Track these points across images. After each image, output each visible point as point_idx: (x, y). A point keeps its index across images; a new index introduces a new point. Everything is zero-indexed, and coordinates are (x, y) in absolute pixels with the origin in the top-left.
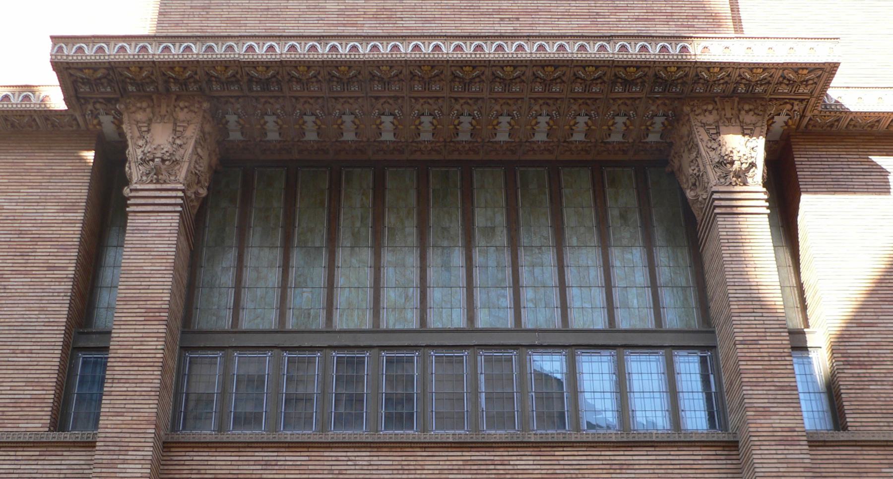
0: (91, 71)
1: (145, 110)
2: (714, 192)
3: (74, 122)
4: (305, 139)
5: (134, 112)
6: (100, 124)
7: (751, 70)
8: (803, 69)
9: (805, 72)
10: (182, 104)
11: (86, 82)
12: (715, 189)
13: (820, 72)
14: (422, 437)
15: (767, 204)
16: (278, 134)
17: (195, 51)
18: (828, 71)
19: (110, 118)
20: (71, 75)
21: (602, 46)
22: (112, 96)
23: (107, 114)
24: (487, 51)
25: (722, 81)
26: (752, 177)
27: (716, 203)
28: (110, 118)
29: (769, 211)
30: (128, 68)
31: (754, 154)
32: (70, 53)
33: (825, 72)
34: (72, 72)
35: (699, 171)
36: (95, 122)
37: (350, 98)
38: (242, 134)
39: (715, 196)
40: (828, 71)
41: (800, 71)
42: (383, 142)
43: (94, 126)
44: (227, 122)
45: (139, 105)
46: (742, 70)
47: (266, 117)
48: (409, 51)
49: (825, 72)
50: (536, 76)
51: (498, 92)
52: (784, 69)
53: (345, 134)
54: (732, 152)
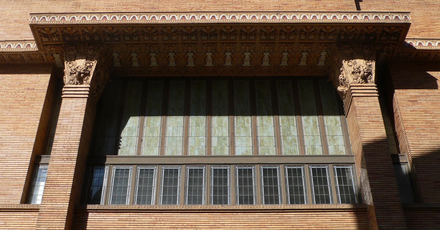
0: (250, 27)
1: (73, 50)
2: (351, 86)
3: (42, 58)
4: (225, 65)
5: (68, 51)
6: (54, 58)
7: (367, 27)
8: (393, 26)
9: (394, 28)
10: (90, 47)
11: (46, 36)
12: (351, 85)
13: (401, 28)
14: (149, 207)
15: (377, 92)
16: (156, 63)
17: (197, 18)
18: (406, 27)
19: (58, 55)
20: (39, 32)
21: (274, 16)
22: (59, 43)
23: (57, 53)
24: (177, 19)
25: (253, 33)
26: (370, 79)
27: (353, 91)
28: (58, 55)
29: (378, 95)
30: (86, 27)
31: (370, 69)
32: (38, 20)
33: (405, 27)
34: (39, 29)
35: (343, 77)
36: (52, 58)
37: (153, 44)
38: (121, 63)
39: (352, 88)
40: (406, 27)
41: (392, 28)
42: (207, 67)
43: (51, 59)
44: (132, 57)
45: (71, 48)
46: (342, 27)
47: (132, 54)
48: (301, 19)
49: (405, 27)
50: (321, 31)
51: (283, 40)
52: (383, 27)
53: (226, 62)
54: (359, 67)
